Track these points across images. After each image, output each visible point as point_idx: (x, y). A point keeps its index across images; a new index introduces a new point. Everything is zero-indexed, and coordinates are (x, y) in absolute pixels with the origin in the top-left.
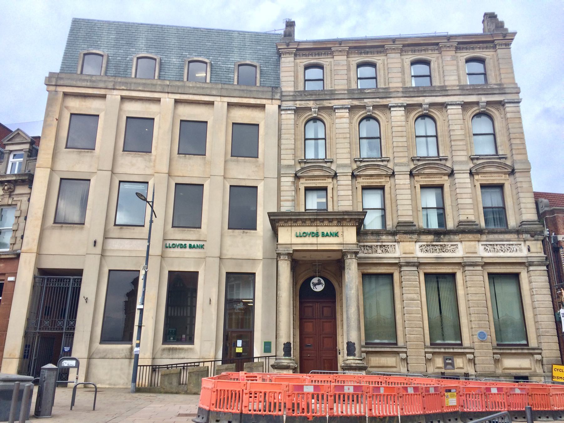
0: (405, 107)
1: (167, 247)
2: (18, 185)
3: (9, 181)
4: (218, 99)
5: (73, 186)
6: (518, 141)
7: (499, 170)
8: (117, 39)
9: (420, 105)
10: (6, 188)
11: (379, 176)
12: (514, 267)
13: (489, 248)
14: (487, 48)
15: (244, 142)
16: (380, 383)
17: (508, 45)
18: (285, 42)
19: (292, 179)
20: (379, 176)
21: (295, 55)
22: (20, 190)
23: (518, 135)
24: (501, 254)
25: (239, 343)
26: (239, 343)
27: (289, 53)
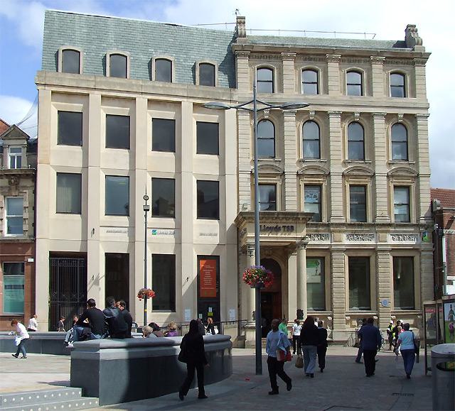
0: (341, 115)
1: (408, 377)
2: (21, 180)
3: (13, 175)
4: (185, 100)
5: (72, 183)
6: (424, 151)
7: (408, 175)
8: (88, 34)
9: (353, 113)
10: (13, 181)
11: (318, 176)
12: (302, 291)
13: (396, 238)
14: (407, 64)
15: (209, 139)
16: (143, 191)
17: (424, 63)
18: (240, 51)
19: (249, 176)
20: (318, 176)
21: (249, 57)
22: (24, 183)
23: (424, 151)
24: (404, 243)
25: (210, 309)
26: (210, 309)
27: (245, 55)
